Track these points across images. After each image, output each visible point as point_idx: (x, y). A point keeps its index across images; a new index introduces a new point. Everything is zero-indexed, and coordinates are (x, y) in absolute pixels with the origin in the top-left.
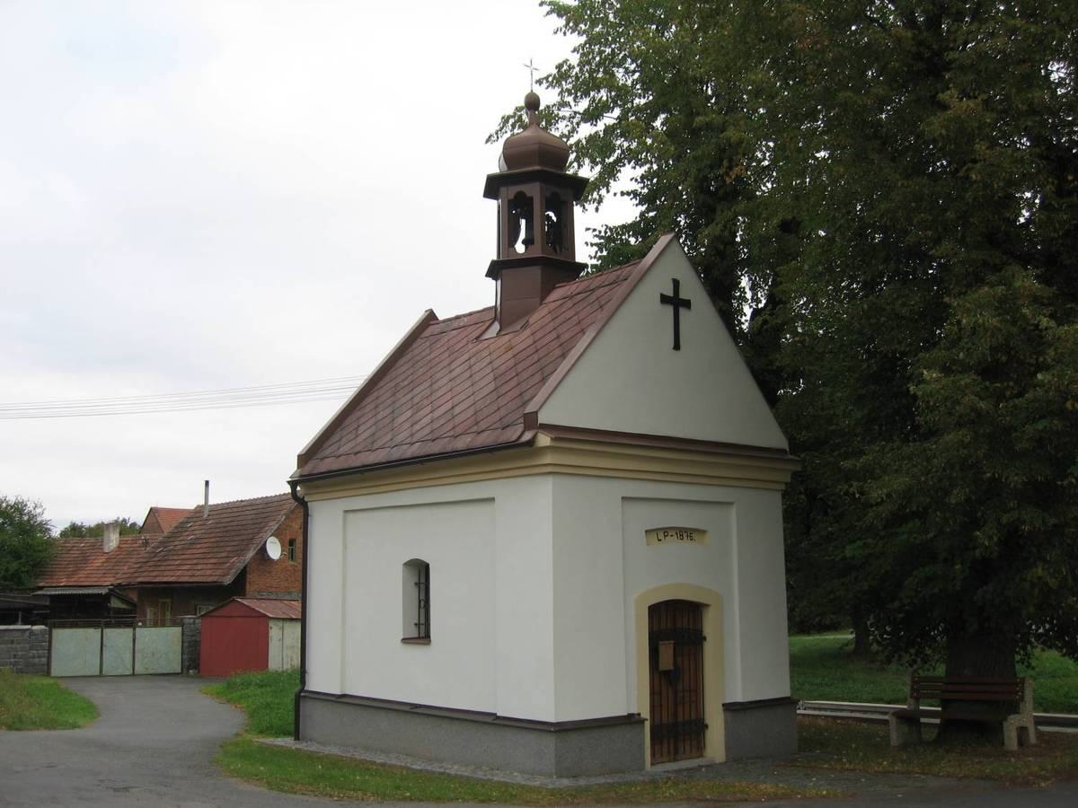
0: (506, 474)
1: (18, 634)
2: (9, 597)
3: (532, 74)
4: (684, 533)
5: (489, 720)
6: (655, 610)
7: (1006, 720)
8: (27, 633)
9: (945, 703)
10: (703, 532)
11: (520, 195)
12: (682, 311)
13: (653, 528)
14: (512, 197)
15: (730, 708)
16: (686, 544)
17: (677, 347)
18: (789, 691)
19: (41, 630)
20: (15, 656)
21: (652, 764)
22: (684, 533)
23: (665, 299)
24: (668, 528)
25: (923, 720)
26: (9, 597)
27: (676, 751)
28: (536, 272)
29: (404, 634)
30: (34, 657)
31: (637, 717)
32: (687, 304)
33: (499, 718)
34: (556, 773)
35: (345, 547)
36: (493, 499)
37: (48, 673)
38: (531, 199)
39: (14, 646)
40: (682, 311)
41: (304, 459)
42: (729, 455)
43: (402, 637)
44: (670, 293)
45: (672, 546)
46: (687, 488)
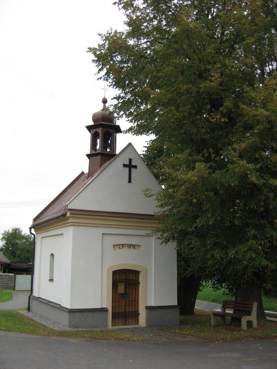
0: (65, 225)
1: (5, 276)
2: (22, 265)
3: (105, 91)
4: (130, 246)
5: (58, 306)
6: (115, 273)
7: (242, 318)
8: (8, 276)
9: (235, 310)
10: (140, 246)
11: (96, 132)
12: (133, 170)
13: (118, 244)
14: (94, 133)
15: (149, 308)
16: (132, 250)
17: (130, 181)
18: (177, 303)
19: (12, 275)
20: (4, 283)
21: (112, 326)
22: (130, 246)
23: (125, 166)
24: (124, 244)
25: (268, 318)
26: (22, 265)
27: (125, 322)
28: (99, 158)
29: (50, 277)
30: (10, 284)
31: (106, 309)
32: (135, 167)
33: (61, 307)
34: (69, 326)
35: (41, 249)
36: (62, 234)
37: (14, 289)
38: (99, 133)
39: (4, 280)
40: (133, 170)
41: (35, 220)
42: (146, 219)
43: (49, 279)
44: (127, 163)
45: (126, 250)
46: (112, 229)
